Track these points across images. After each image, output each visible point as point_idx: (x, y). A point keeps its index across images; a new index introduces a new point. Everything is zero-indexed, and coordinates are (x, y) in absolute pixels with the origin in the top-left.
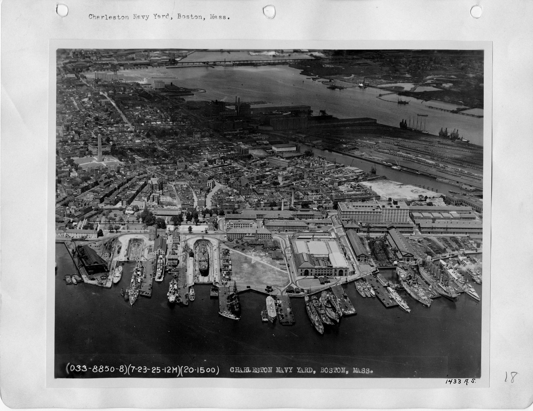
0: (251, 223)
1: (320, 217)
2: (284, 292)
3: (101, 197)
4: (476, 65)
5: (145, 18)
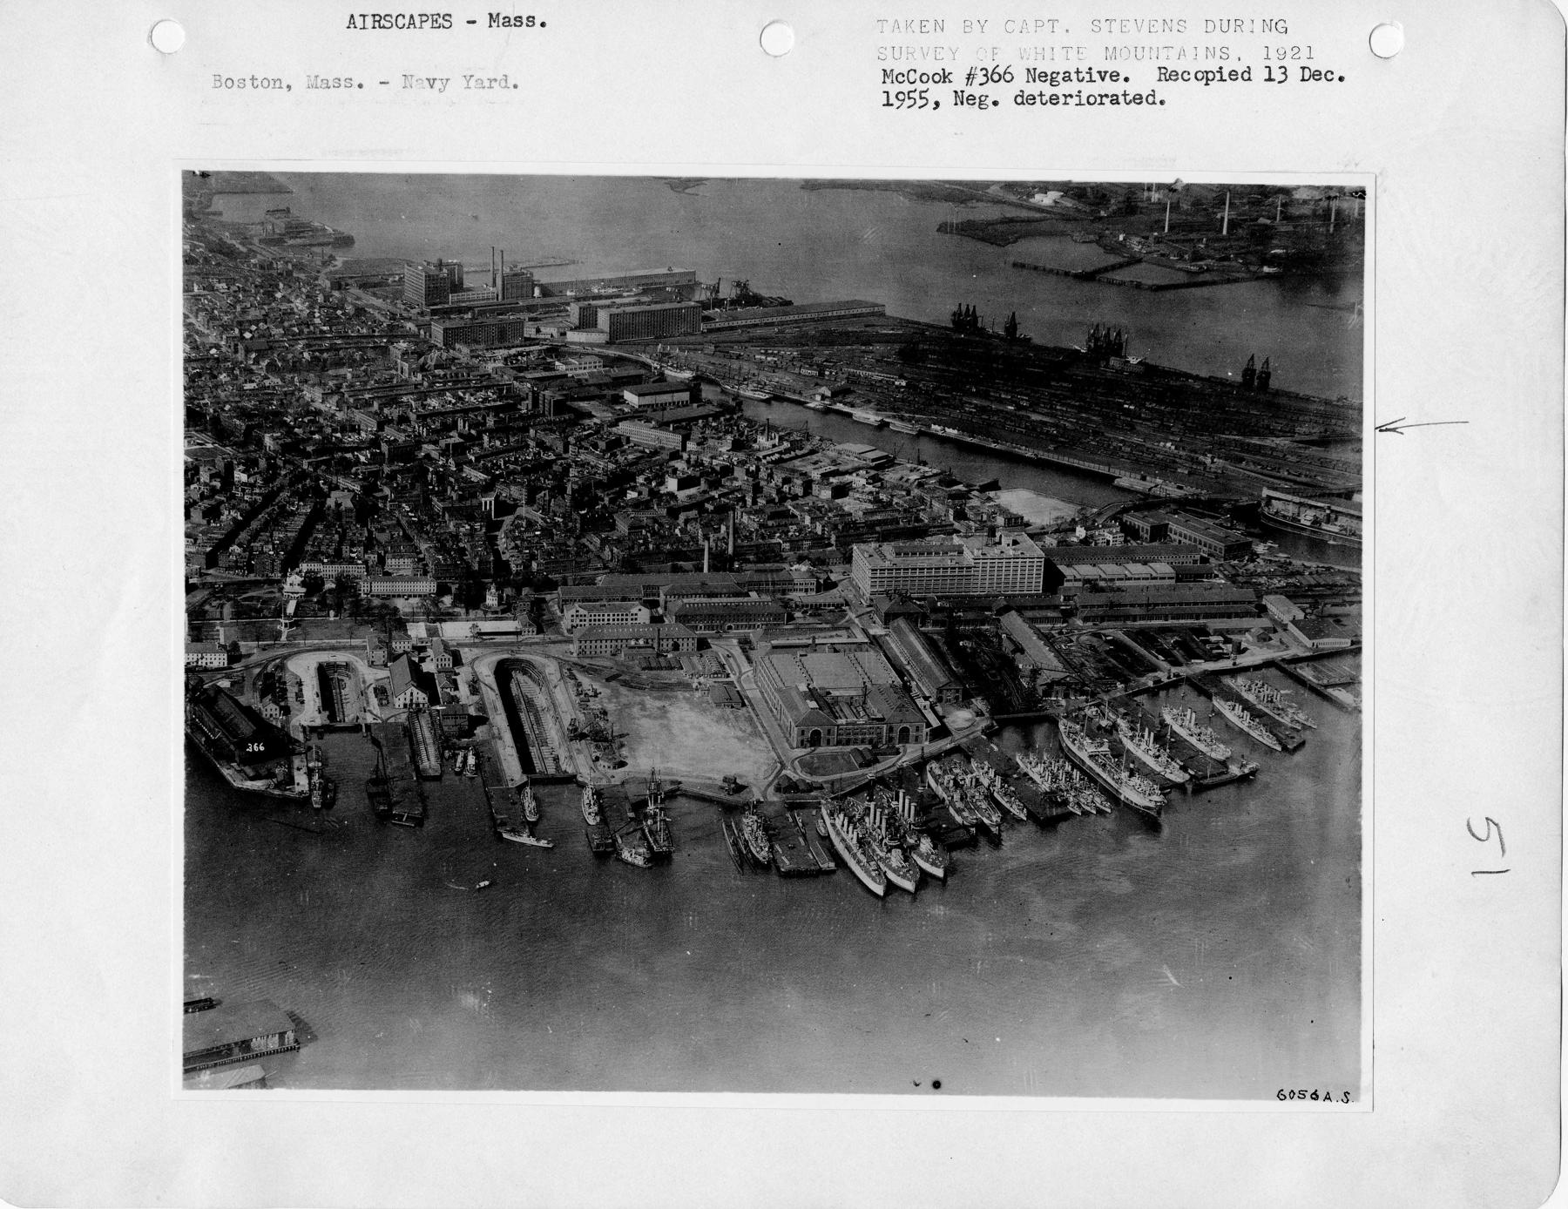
0: (634, 611)
1: (809, 587)
2: (771, 789)
3: (208, 549)
4: (1358, 238)
5: (438, 84)
